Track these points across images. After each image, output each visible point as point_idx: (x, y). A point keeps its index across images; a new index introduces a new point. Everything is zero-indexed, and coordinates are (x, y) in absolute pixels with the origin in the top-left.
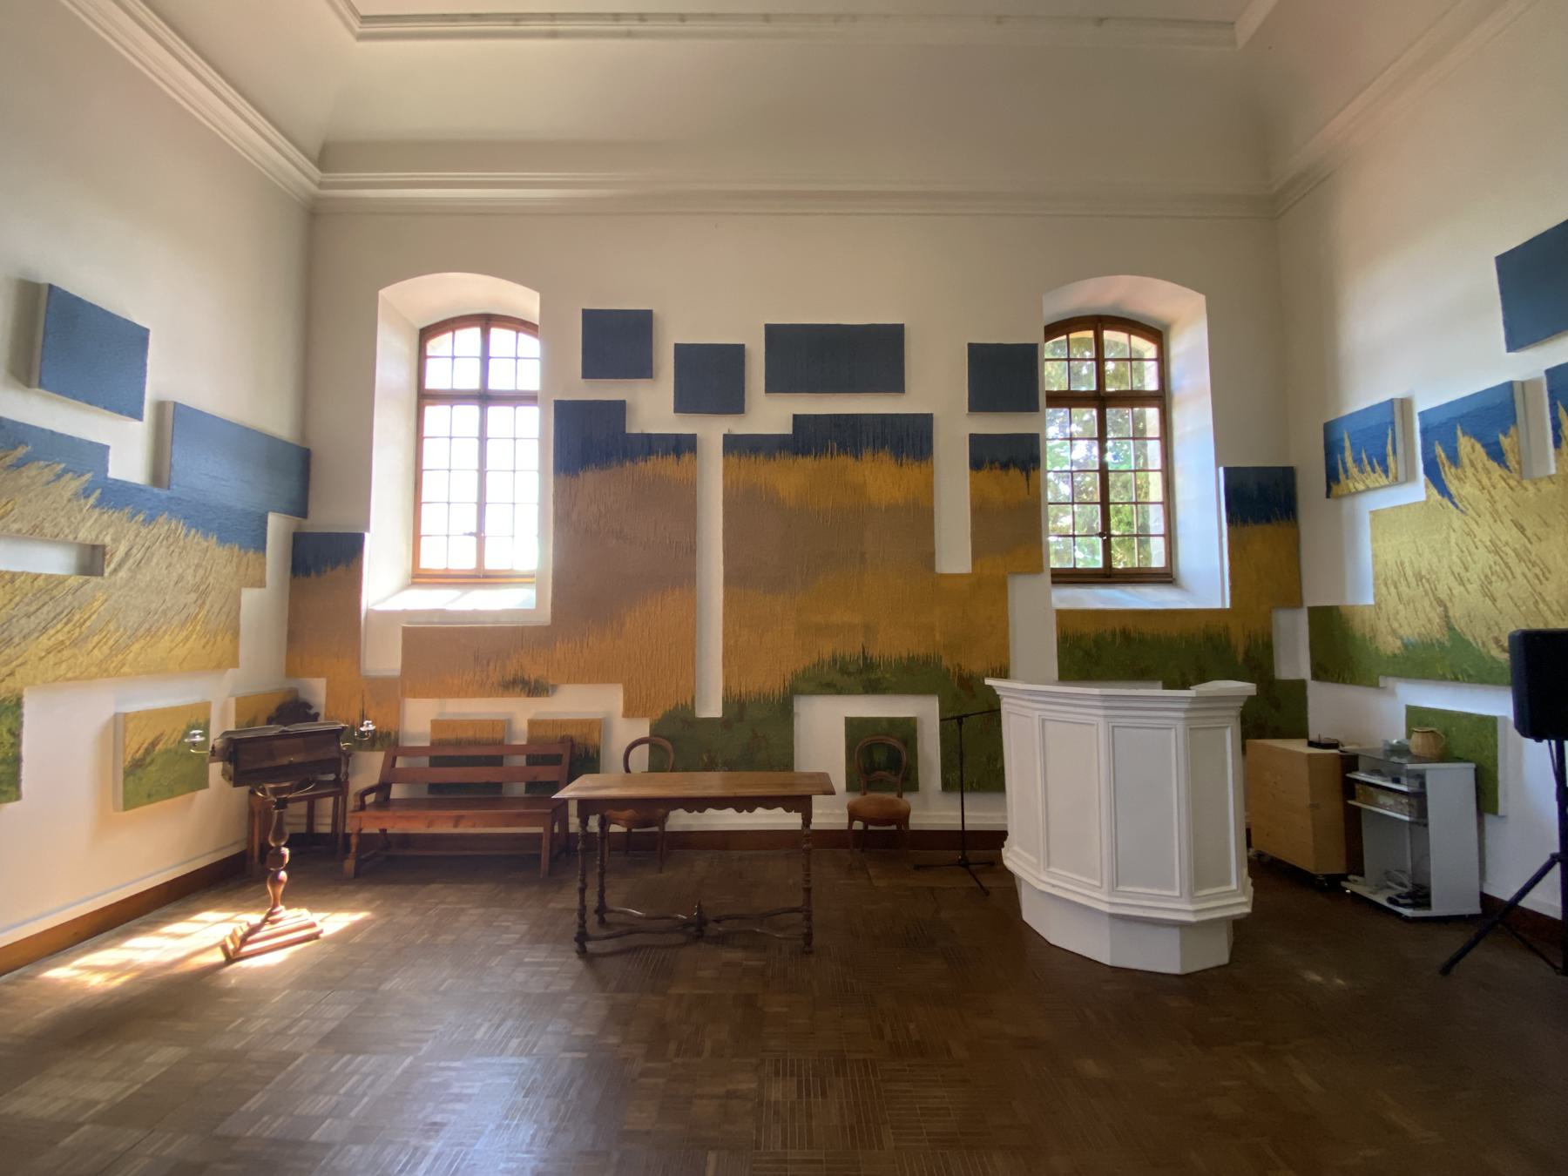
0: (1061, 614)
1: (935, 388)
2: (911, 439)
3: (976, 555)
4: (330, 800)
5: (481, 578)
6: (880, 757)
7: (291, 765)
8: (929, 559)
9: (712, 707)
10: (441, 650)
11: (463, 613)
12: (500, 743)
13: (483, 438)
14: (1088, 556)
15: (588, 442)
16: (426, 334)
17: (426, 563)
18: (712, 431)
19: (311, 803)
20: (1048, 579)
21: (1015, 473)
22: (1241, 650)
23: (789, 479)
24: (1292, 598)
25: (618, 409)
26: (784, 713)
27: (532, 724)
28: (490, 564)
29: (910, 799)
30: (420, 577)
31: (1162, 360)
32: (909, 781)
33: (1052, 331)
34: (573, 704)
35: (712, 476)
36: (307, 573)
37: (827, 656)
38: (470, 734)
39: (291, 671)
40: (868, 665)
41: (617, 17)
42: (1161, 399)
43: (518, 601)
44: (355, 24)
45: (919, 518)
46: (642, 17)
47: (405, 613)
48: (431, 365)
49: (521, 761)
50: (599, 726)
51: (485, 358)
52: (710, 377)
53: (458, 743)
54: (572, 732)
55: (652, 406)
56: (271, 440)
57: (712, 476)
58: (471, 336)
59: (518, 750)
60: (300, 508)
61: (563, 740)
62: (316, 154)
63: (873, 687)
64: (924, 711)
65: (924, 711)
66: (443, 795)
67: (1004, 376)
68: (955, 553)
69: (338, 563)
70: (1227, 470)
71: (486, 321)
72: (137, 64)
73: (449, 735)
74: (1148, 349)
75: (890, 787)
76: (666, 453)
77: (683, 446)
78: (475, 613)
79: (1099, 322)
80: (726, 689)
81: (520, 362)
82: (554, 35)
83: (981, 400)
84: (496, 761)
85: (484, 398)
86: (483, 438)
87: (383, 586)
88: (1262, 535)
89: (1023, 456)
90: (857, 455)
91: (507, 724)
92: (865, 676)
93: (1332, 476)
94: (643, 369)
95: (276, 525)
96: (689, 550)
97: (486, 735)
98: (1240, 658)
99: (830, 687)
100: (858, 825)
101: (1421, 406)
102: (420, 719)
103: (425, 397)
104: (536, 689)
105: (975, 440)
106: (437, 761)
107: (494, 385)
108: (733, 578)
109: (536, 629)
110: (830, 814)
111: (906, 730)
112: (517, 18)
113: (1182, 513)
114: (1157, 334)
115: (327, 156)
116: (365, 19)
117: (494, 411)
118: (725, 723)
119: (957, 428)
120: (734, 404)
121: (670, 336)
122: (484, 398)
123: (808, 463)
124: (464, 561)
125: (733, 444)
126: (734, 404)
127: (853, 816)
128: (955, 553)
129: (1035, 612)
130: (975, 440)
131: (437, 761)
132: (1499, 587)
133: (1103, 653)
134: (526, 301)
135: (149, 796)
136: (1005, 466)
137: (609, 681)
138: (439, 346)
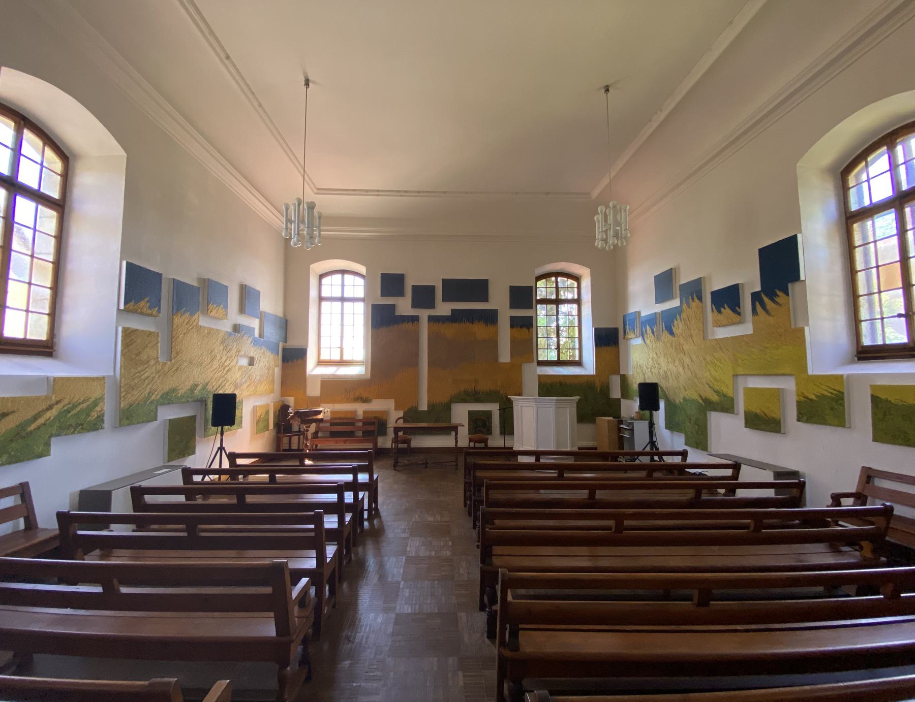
1: (499, 300)
2: (490, 317)
3: (512, 356)
4: (297, 437)
5: (341, 363)
6: (479, 423)
9: (424, 407)
11: (341, 376)
12: (353, 419)
14: (553, 356)
15: (382, 319)
16: (322, 276)
17: (323, 358)
18: (424, 314)
19: (290, 437)
20: (536, 363)
21: (525, 329)
23: (450, 330)
24: (616, 370)
25: (393, 307)
26: (448, 409)
27: (364, 412)
28: (345, 358)
29: (490, 437)
30: (321, 363)
31: (579, 288)
32: (489, 431)
33: (539, 278)
34: (377, 405)
36: (288, 361)
37: (462, 389)
39: (283, 394)
41: (398, 191)
42: (578, 301)
43: (356, 371)
44: (315, 191)
45: (493, 345)
46: (406, 192)
47: (322, 375)
48: (323, 288)
49: (361, 424)
50: (386, 413)
51: (343, 285)
52: (424, 297)
53: (340, 418)
55: (404, 306)
56: (276, 316)
58: (338, 277)
59: (360, 421)
60: (286, 342)
61: (376, 418)
64: (494, 408)
65: (494, 408)
66: (334, 435)
67: (523, 297)
68: (505, 357)
70: (596, 329)
71: (343, 272)
72: (754, 627)
75: (483, 433)
77: (415, 319)
79: (557, 274)
80: (429, 402)
81: (356, 287)
83: (514, 305)
84: (352, 424)
85: (343, 299)
86: (342, 314)
87: (312, 368)
89: (528, 324)
90: (473, 322)
91: (355, 412)
92: (477, 399)
93: (625, 333)
94: (401, 293)
95: (281, 345)
96: (416, 355)
97: (349, 416)
99: (464, 401)
100: (472, 444)
101: (643, 314)
102: (326, 411)
103: (321, 299)
104: (366, 401)
105: (512, 318)
106: (332, 424)
107: (346, 295)
110: (464, 440)
111: (488, 414)
112: (367, 191)
113: (584, 342)
114: (577, 279)
116: (318, 189)
117: (346, 304)
118: (428, 412)
119: (506, 313)
123: (456, 325)
124: (336, 357)
125: (431, 319)
126: (431, 305)
127: (471, 440)
128: (505, 357)
129: (532, 375)
130: (512, 318)
131: (332, 424)
133: (551, 388)
134: (362, 269)
136: (521, 327)
138: (325, 281)
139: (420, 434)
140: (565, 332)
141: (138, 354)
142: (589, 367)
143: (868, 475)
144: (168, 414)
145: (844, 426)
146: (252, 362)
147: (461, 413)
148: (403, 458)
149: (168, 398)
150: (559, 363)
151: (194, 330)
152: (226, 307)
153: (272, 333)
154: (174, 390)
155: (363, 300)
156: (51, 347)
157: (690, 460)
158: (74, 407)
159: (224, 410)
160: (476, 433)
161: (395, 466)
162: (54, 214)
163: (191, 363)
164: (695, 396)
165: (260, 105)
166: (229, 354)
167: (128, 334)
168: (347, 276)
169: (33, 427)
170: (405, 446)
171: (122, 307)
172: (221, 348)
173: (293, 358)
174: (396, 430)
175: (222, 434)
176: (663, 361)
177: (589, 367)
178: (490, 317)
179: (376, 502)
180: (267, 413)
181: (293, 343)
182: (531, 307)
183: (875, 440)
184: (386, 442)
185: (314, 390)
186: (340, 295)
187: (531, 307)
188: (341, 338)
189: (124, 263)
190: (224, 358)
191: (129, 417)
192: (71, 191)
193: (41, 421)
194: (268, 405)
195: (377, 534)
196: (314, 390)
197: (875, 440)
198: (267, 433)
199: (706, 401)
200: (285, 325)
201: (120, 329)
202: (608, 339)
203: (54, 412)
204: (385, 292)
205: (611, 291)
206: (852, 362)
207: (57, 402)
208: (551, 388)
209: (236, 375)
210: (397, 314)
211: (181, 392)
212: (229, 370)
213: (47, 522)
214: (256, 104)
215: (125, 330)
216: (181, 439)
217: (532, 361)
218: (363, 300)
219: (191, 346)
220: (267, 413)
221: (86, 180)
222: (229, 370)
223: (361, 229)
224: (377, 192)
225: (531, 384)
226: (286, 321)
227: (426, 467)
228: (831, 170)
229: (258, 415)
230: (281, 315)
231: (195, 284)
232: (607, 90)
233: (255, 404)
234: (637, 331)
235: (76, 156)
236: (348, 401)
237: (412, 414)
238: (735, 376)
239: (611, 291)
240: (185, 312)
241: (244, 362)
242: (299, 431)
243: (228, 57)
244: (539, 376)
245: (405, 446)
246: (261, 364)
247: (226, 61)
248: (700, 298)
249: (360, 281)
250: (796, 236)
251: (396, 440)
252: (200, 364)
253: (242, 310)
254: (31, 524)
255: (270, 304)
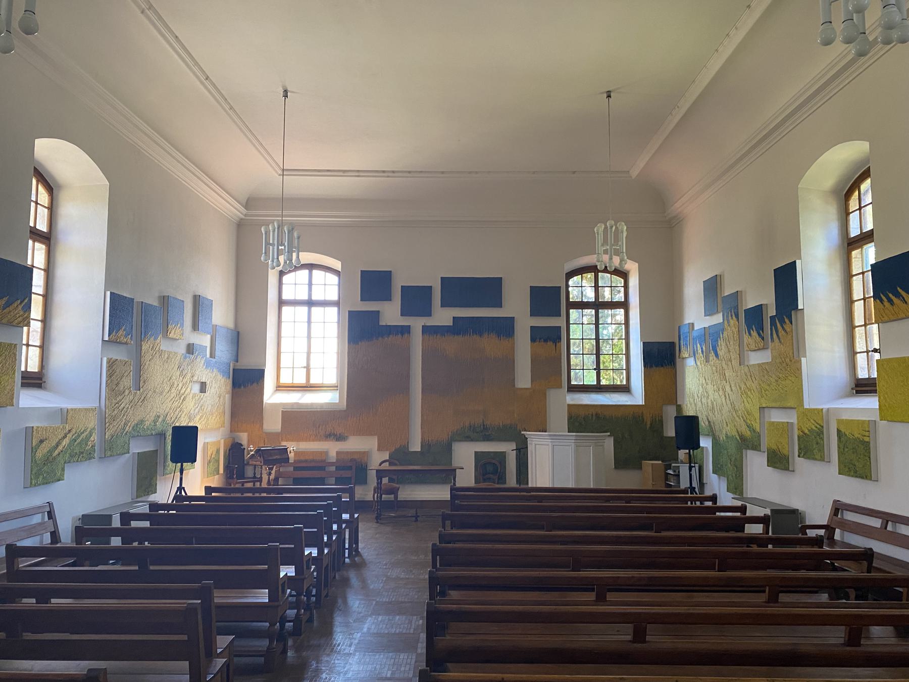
0: (570, 406)
1: (515, 304)
2: (505, 327)
3: (532, 382)
5: (308, 387)
7: (276, 459)
8: (513, 381)
9: (416, 447)
10: (297, 420)
11: (307, 405)
12: (324, 461)
13: (309, 322)
14: (590, 379)
15: (361, 329)
18: (417, 324)
21: (550, 344)
22: (649, 423)
23: (451, 345)
26: (448, 450)
27: (338, 453)
30: (280, 387)
31: (626, 286)
34: (355, 444)
35: (417, 340)
36: (239, 387)
37: (467, 424)
38: (311, 458)
40: (485, 428)
42: (624, 305)
45: (508, 364)
46: (393, 172)
49: (333, 468)
50: (366, 454)
51: (310, 284)
52: (416, 300)
53: (306, 461)
54: (355, 457)
55: (391, 313)
57: (417, 340)
59: (332, 464)
61: (352, 460)
62: (244, 202)
63: (487, 438)
65: (508, 448)
67: (549, 301)
68: (524, 380)
69: (253, 382)
71: (311, 267)
73: (302, 458)
74: (621, 281)
76: (397, 334)
78: (312, 404)
81: (327, 286)
82: (358, 176)
83: (535, 311)
84: (322, 468)
85: (310, 303)
86: (309, 322)
87: (271, 396)
88: (660, 372)
91: (326, 453)
92: (485, 434)
94: (388, 297)
96: (406, 377)
98: (648, 426)
103: (282, 303)
104: (340, 438)
108: (426, 389)
109: (340, 411)
111: (502, 456)
112: (344, 171)
114: (624, 275)
115: (250, 203)
117: (314, 310)
118: (421, 453)
119: (525, 323)
120: (426, 311)
121: (398, 283)
122: (310, 303)
123: (459, 338)
124: (301, 379)
125: (426, 330)
126: (426, 311)
128: (524, 380)
131: (296, 469)
132: (704, 400)
133: (583, 422)
134: (337, 265)
135: (330, 435)
136: (546, 341)
137: (372, 435)
138: (286, 279)
139: (412, 483)
140: (605, 351)
141: (117, 385)
142: (637, 397)
143: (838, 508)
144: (138, 447)
145: (823, 460)
146: (203, 387)
147: (465, 455)
148: (388, 510)
149: (138, 432)
150: (598, 388)
151: (157, 355)
152: (182, 325)
153: (223, 351)
154: (142, 421)
155: (336, 304)
156: (41, 379)
157: (749, 514)
158: (79, 436)
159: (184, 443)
160: (485, 481)
161: (377, 518)
162: (44, 246)
163: (155, 392)
164: (735, 433)
165: (231, 108)
166: (185, 380)
167: (111, 364)
168: (315, 272)
169: (56, 452)
170: (391, 497)
171: (106, 338)
172: (178, 373)
173: (245, 381)
174: (380, 474)
175: (181, 473)
176: (710, 388)
177: (637, 397)
178: (505, 327)
179: (357, 543)
180: (218, 451)
181: (248, 362)
182: (559, 314)
183: (840, 474)
184: (365, 493)
185: (273, 424)
186: (306, 297)
187: (559, 314)
188: (308, 353)
189: (108, 293)
190: (180, 385)
191: (111, 449)
192: (56, 224)
193: (60, 448)
194: (219, 442)
195: (359, 565)
196: (273, 424)
197: (840, 474)
198: (217, 477)
199: (742, 437)
200: (237, 338)
201: (105, 360)
202: (661, 357)
203: (65, 442)
204: (366, 295)
205: (664, 295)
206: (850, 395)
207: (70, 431)
208: (583, 422)
209: (190, 405)
210: (382, 323)
211: (147, 423)
212: (184, 400)
213: (67, 538)
214: (227, 107)
215: (109, 361)
216: (146, 474)
217: (560, 386)
218: (336, 304)
219: (157, 373)
220: (218, 451)
221: (69, 210)
222: (184, 400)
223: (334, 213)
224: (358, 173)
225: (558, 417)
226: (238, 333)
227: (416, 521)
228: (835, 191)
229: (209, 453)
230: (231, 325)
231: (156, 304)
232: (609, 96)
233: (210, 441)
234: (690, 349)
235: (59, 187)
236: (317, 438)
237: (400, 455)
238: (762, 409)
239: (664, 295)
240: (151, 336)
241: (196, 388)
242: (255, 477)
243: (207, 78)
244: (569, 405)
245: (391, 497)
246: (213, 390)
247: (207, 83)
248: (737, 316)
249: (333, 279)
250: (795, 262)
251: (378, 489)
252: (161, 393)
253: (195, 327)
254: (55, 536)
255: (221, 315)
